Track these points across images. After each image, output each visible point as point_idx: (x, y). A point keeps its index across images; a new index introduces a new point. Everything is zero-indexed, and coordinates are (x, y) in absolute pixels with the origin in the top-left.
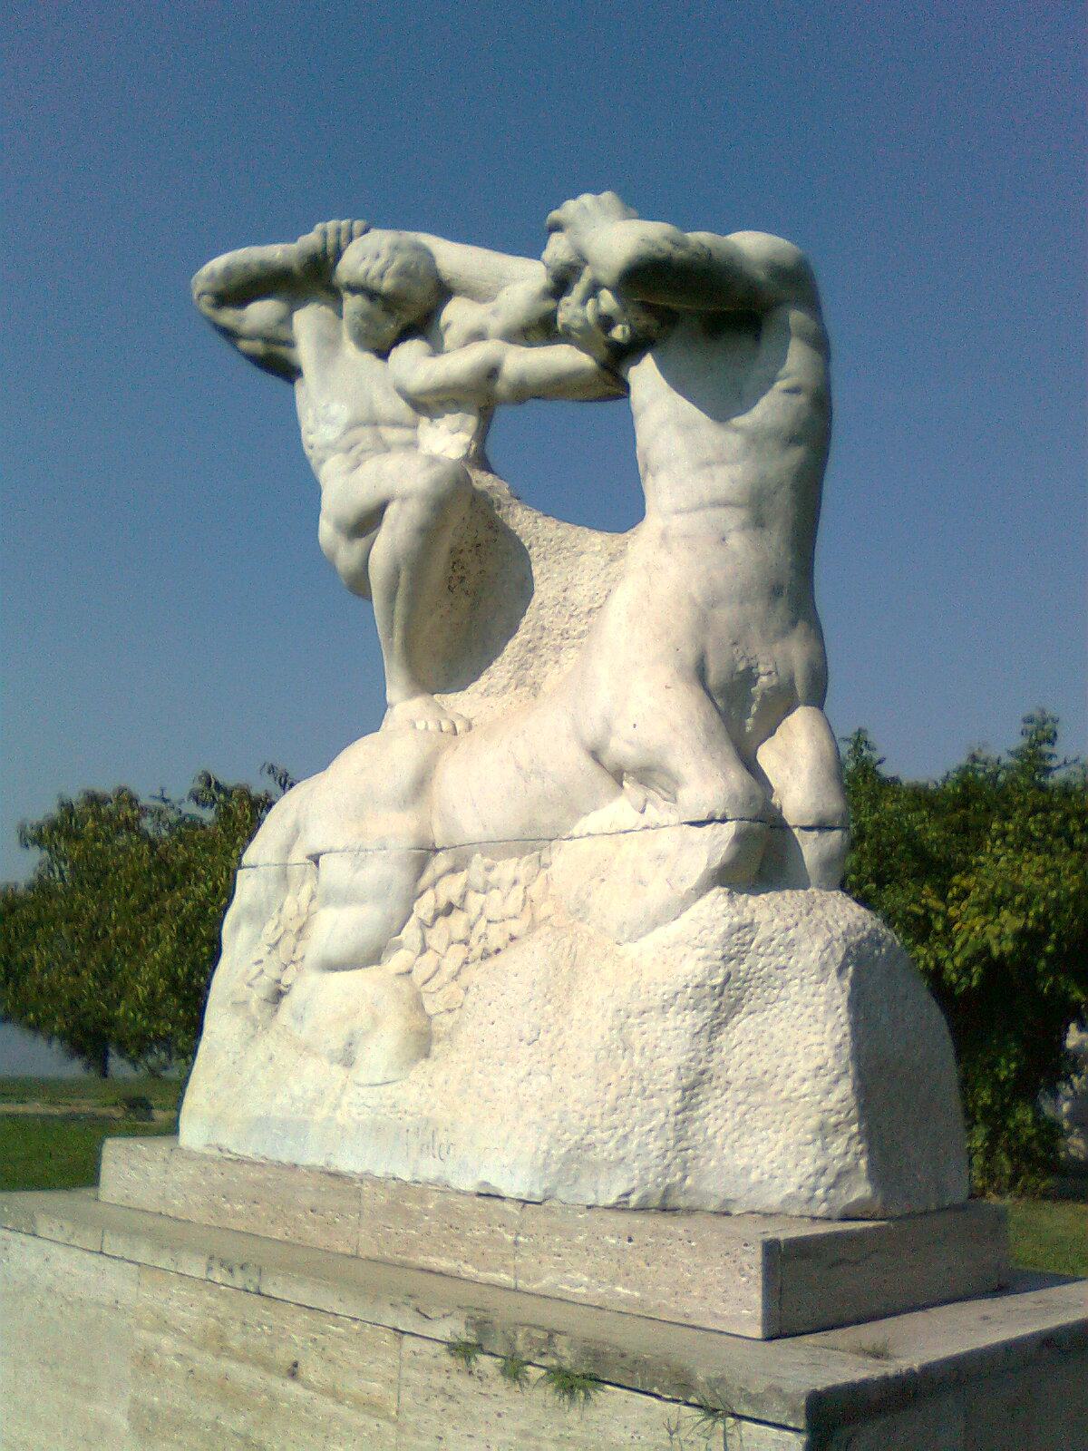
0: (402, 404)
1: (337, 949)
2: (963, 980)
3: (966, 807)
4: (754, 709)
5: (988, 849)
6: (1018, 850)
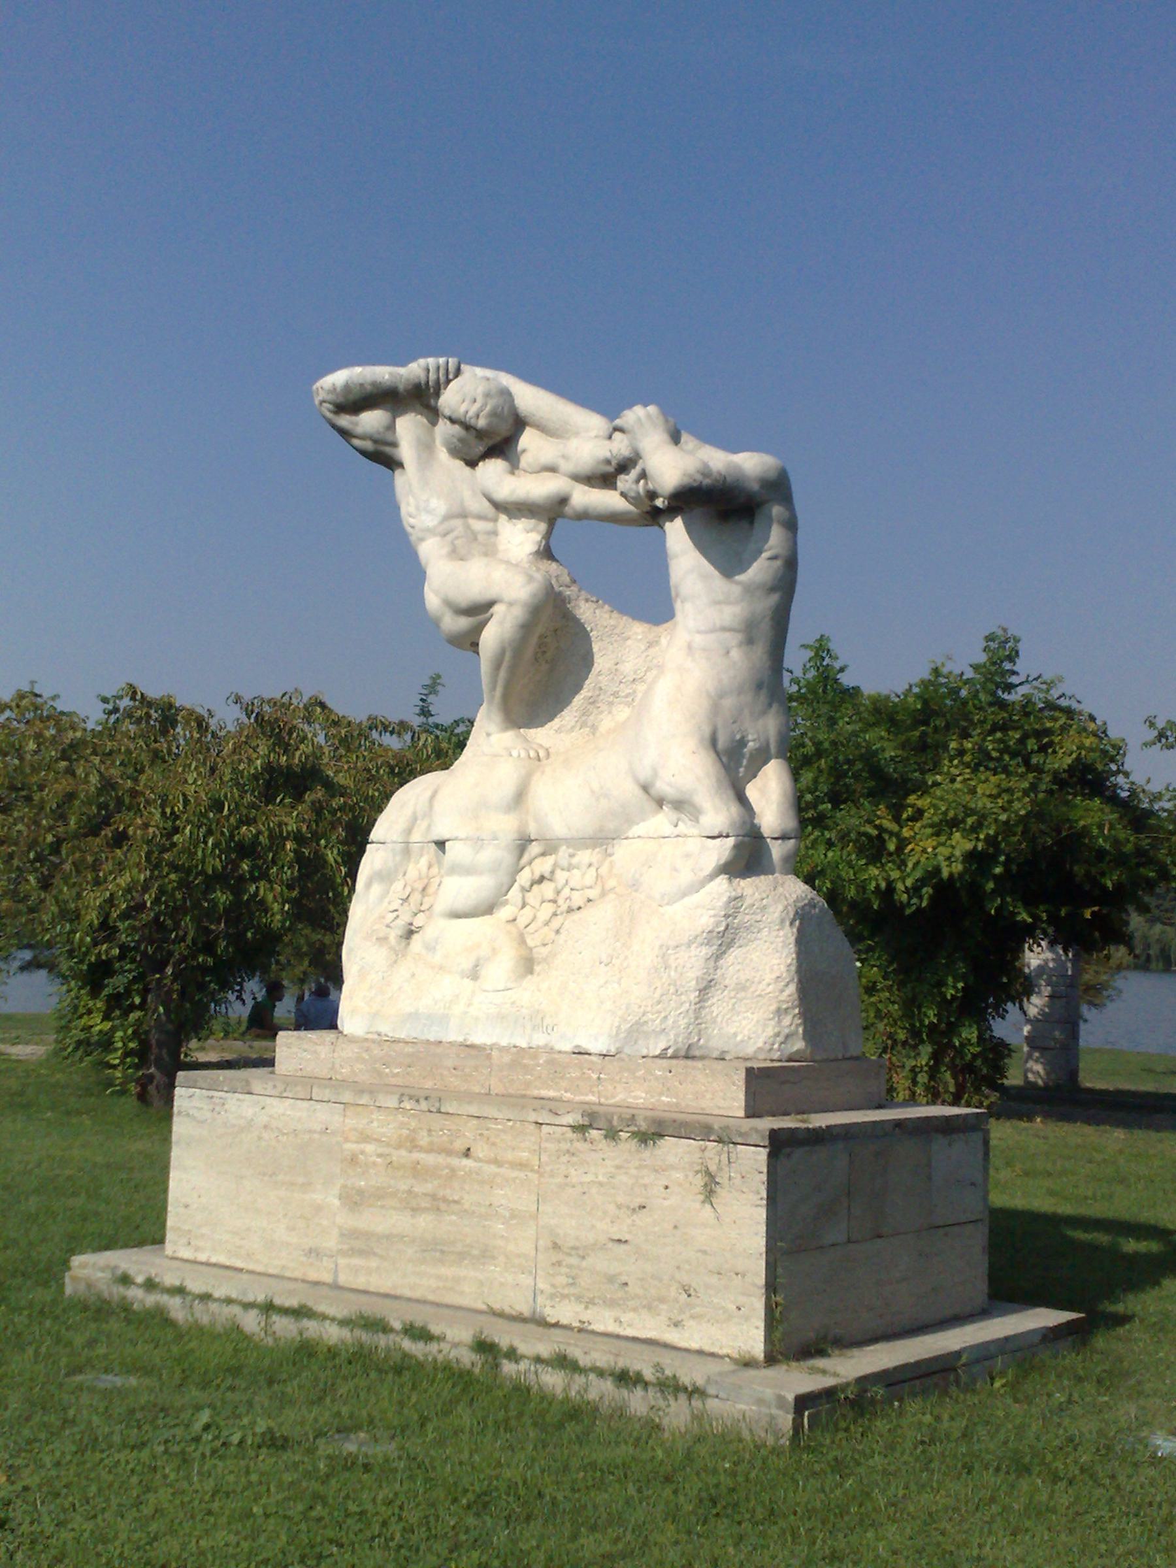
0: (487, 504)
1: (461, 904)
2: (914, 901)
3: (926, 723)
4: (745, 762)
5: (946, 769)
6: (975, 770)
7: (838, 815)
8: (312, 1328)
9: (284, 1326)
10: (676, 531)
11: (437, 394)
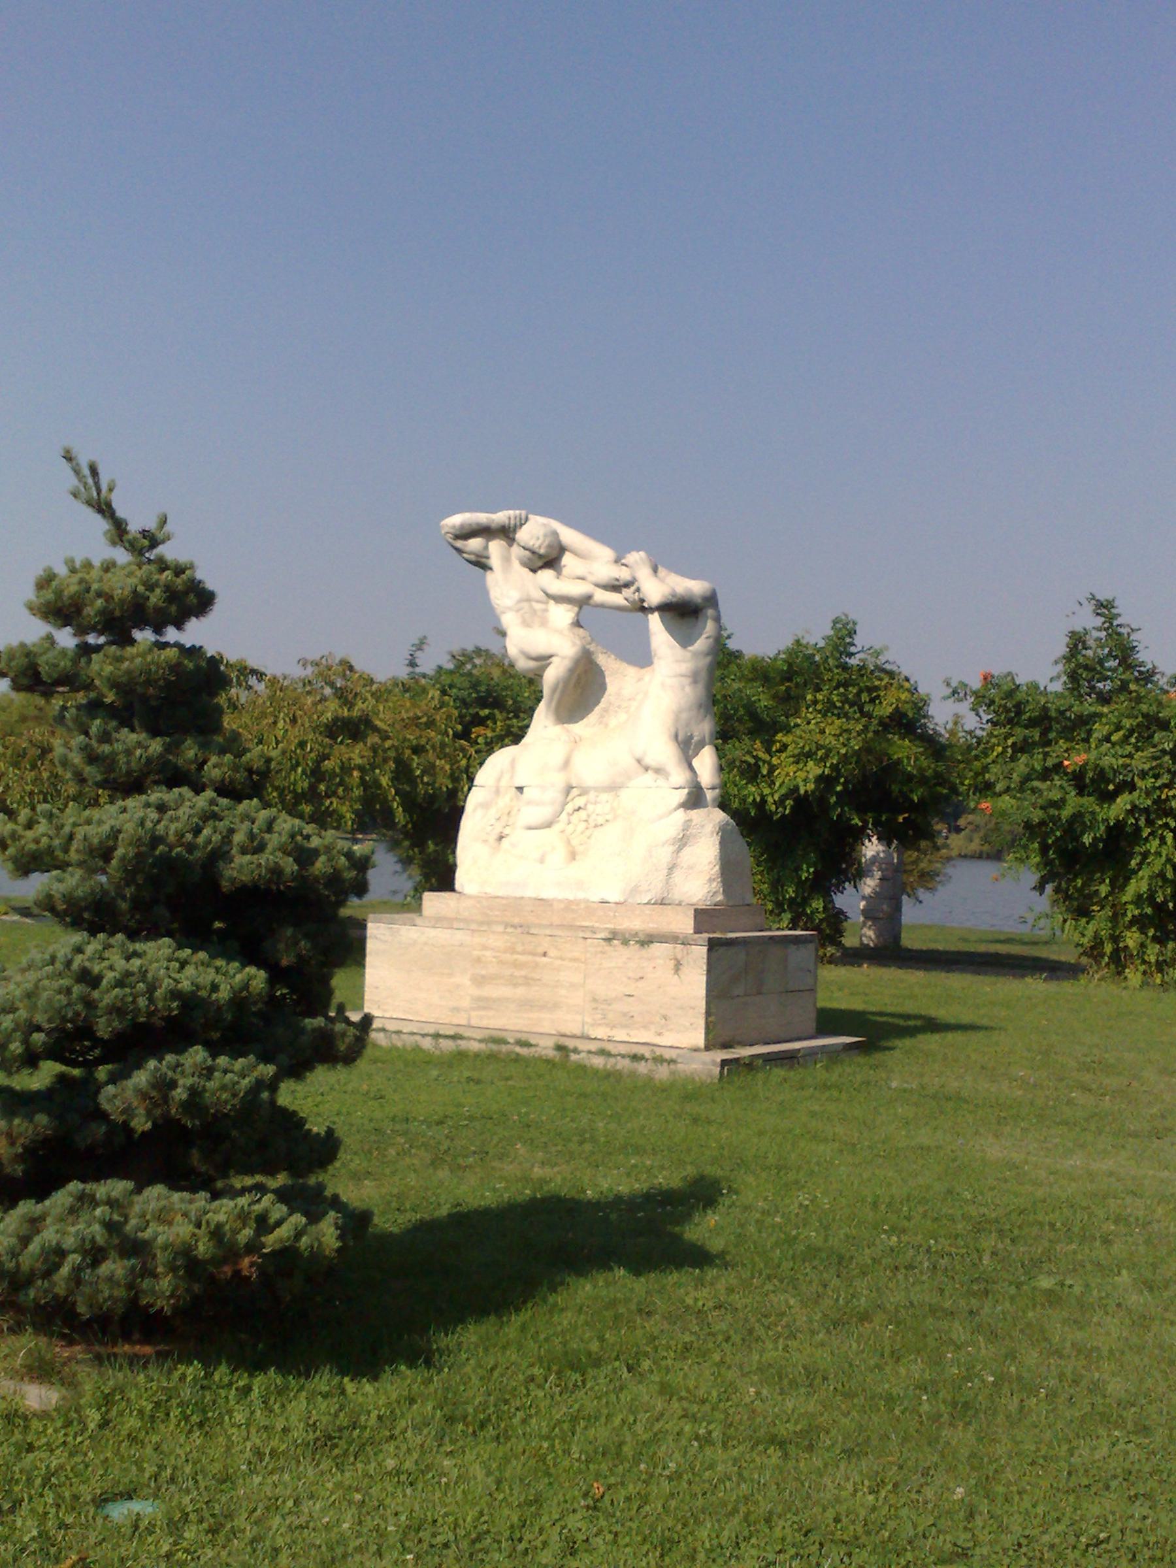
1: (533, 822)
2: (780, 809)
3: (789, 679)
6: (824, 716)
7: (727, 747)
8: (463, 1044)
9: (447, 1045)
10: (655, 620)
11: (515, 531)
